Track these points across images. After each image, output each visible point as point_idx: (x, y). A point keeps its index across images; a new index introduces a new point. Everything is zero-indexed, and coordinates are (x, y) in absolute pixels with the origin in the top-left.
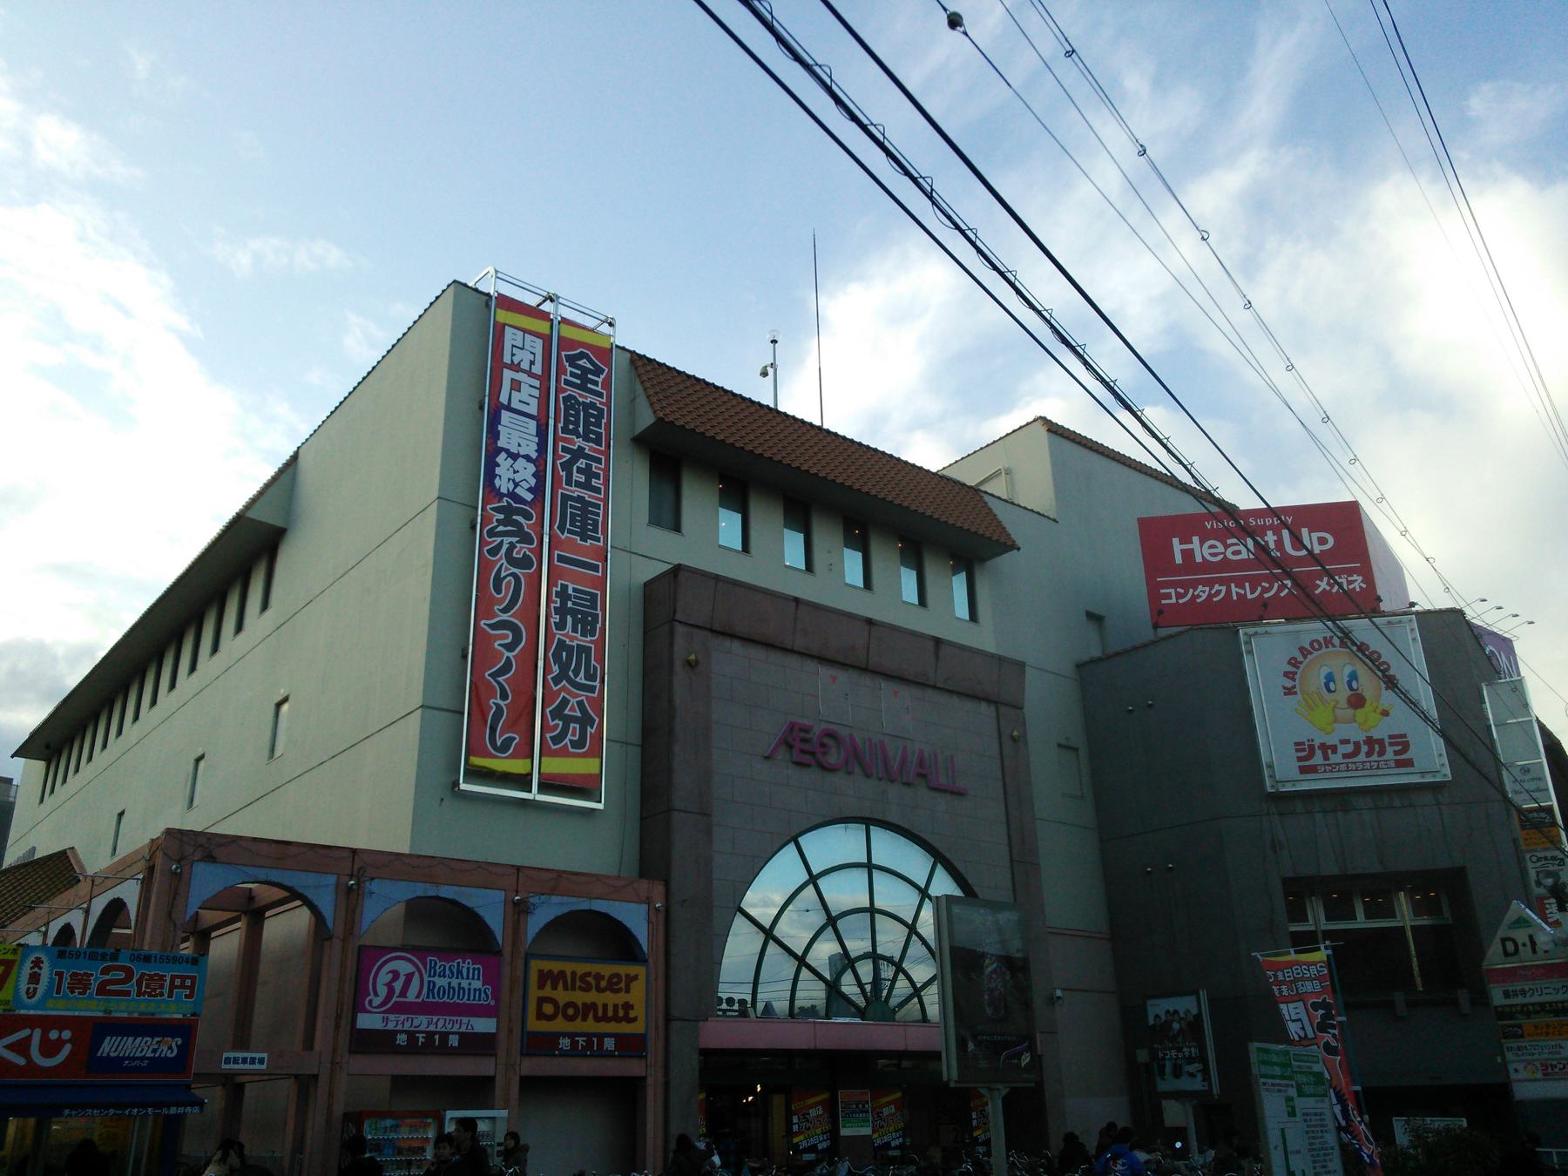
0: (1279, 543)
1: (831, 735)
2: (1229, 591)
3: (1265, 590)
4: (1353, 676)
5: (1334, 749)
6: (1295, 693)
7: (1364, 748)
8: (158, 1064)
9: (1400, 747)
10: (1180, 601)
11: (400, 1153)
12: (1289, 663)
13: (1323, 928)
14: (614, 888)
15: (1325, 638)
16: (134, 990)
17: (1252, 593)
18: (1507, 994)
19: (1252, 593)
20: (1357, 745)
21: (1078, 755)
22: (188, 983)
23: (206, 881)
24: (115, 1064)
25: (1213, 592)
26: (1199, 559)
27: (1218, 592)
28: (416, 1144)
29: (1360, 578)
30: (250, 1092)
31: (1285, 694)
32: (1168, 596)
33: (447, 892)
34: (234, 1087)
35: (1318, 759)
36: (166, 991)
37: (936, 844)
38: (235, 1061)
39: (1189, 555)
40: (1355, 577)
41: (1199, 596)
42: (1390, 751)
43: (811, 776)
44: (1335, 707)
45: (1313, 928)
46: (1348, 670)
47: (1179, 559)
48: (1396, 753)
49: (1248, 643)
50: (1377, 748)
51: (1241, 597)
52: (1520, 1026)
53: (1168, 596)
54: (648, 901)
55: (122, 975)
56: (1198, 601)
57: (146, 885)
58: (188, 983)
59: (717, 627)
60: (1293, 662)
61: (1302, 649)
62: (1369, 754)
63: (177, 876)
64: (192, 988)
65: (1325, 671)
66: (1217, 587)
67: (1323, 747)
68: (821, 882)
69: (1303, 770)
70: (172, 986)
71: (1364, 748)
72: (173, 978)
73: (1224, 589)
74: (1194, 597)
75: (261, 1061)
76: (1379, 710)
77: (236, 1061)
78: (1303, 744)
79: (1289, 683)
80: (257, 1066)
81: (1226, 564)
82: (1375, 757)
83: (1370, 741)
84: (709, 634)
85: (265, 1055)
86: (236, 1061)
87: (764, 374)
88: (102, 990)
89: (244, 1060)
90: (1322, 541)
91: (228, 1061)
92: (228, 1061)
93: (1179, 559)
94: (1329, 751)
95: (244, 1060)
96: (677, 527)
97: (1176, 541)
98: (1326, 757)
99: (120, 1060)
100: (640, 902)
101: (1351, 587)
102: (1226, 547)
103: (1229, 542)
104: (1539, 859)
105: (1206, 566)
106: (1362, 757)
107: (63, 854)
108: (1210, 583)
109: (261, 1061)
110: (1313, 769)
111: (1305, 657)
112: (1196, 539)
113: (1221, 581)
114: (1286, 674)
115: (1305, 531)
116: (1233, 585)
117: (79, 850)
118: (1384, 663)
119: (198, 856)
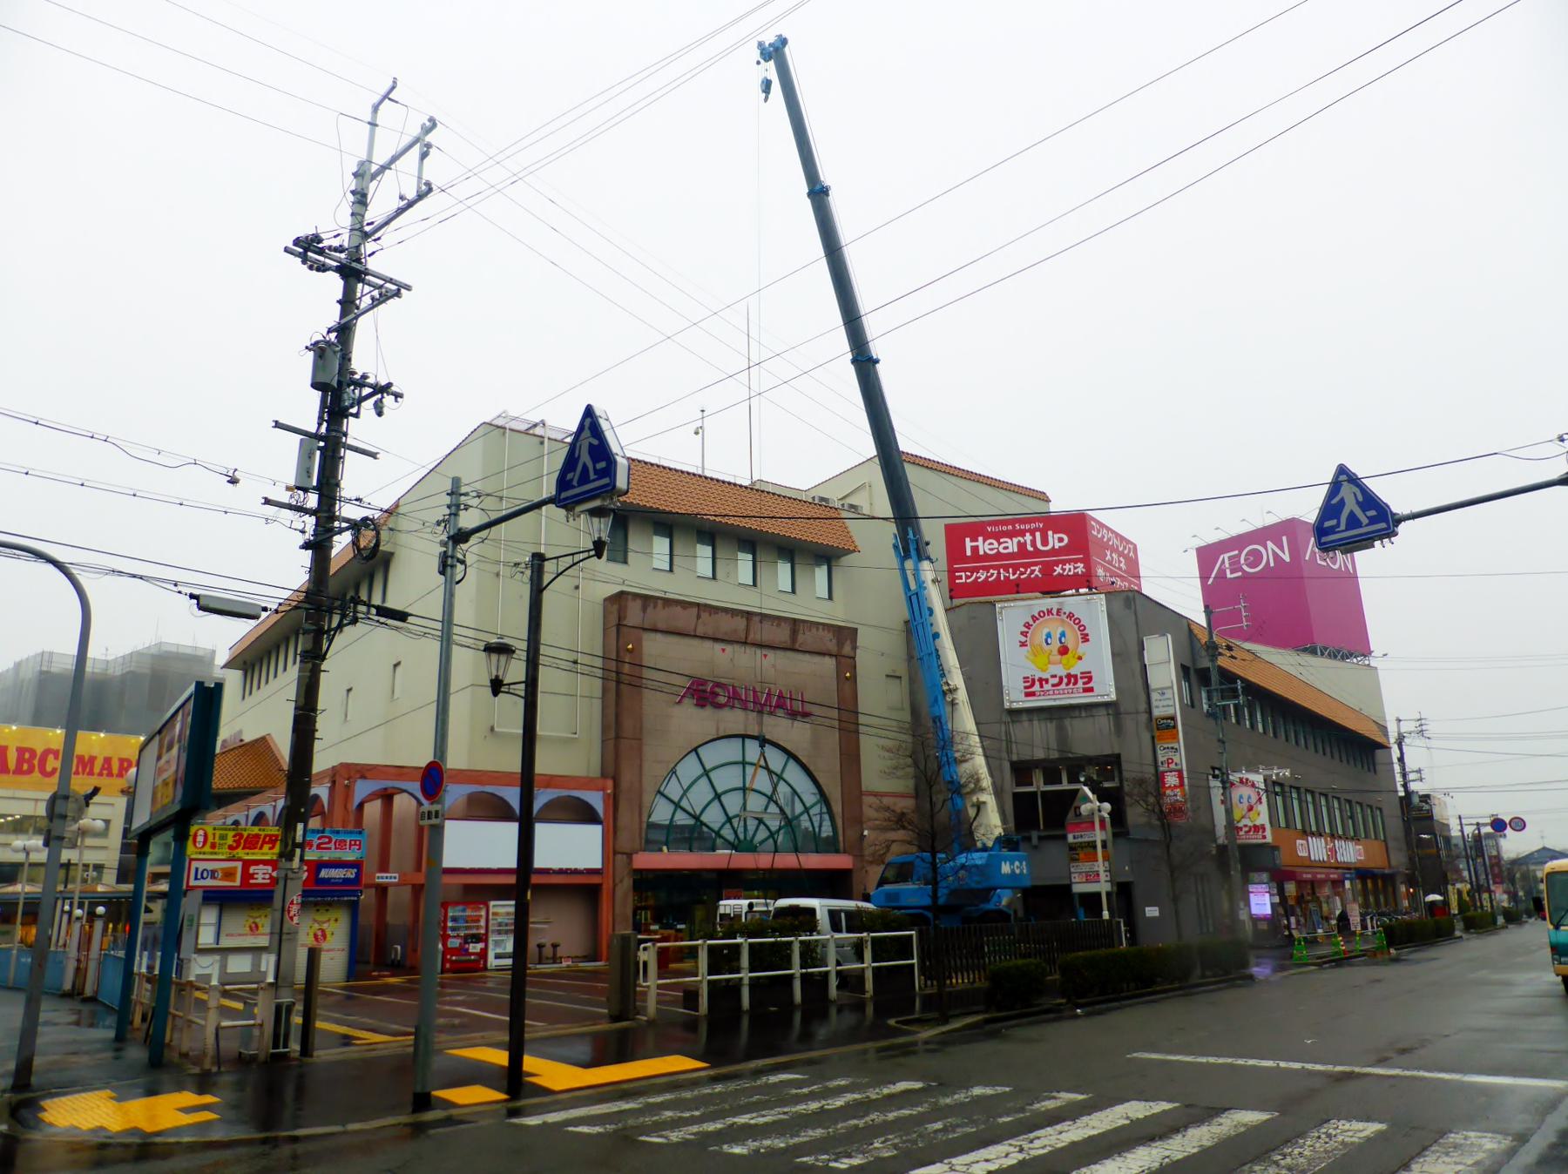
0: (1033, 543)
1: (718, 685)
2: (999, 573)
3: (1022, 573)
4: (1063, 634)
5: (1047, 681)
6: (1026, 645)
7: (1065, 680)
8: (346, 881)
9: (1087, 680)
10: (968, 581)
11: (467, 922)
12: (1025, 626)
13: (1042, 789)
14: (586, 783)
15: (1048, 610)
16: (333, 847)
17: (1014, 574)
18: (1074, 838)
19: (1014, 574)
20: (1061, 679)
21: (901, 683)
22: (358, 843)
23: (362, 789)
24: (327, 881)
25: (989, 574)
26: (981, 553)
27: (992, 575)
28: (474, 918)
29: (1082, 565)
30: (391, 891)
31: (1021, 646)
32: (961, 578)
33: (489, 789)
34: (382, 890)
35: (1037, 687)
36: (348, 847)
37: (789, 748)
38: (382, 878)
39: (975, 549)
40: (1079, 564)
41: (980, 578)
42: (1080, 682)
43: (708, 711)
44: (1050, 654)
45: (1035, 790)
46: (1060, 630)
47: (969, 553)
48: (1084, 683)
49: (1001, 613)
50: (1073, 680)
51: (1007, 578)
52: (1078, 854)
53: (961, 578)
54: (603, 789)
55: (327, 840)
56: (979, 580)
57: (332, 790)
58: (358, 843)
59: (646, 626)
60: (1028, 626)
61: (1033, 617)
62: (1068, 684)
63: (347, 787)
64: (360, 845)
65: (1046, 631)
66: (991, 571)
67: (1041, 680)
68: (712, 775)
69: (1028, 695)
70: (350, 845)
71: (1065, 680)
72: (351, 841)
73: (996, 572)
74: (977, 578)
75: (395, 878)
76: (1076, 656)
77: (382, 878)
78: (1028, 678)
79: (1023, 639)
80: (393, 880)
81: (999, 556)
82: (1071, 686)
83: (1069, 676)
84: (641, 631)
85: (397, 875)
86: (382, 878)
87: (697, 433)
88: (319, 847)
89: (387, 878)
90: (1061, 540)
91: (378, 878)
92: (378, 878)
93: (969, 553)
94: (1044, 683)
95: (387, 878)
96: (625, 562)
97: (968, 540)
98: (1042, 686)
99: (329, 879)
100: (598, 790)
101: (1076, 571)
102: (1000, 544)
103: (1002, 540)
104: (1164, 749)
105: (986, 557)
106: (1063, 686)
107: (263, 738)
108: (987, 569)
109: (395, 878)
110: (1033, 694)
111: (1034, 622)
112: (981, 539)
113: (997, 568)
114: (1022, 633)
115: (1050, 533)
116: (1002, 571)
117: (274, 735)
118: (1083, 625)
119: (358, 776)
